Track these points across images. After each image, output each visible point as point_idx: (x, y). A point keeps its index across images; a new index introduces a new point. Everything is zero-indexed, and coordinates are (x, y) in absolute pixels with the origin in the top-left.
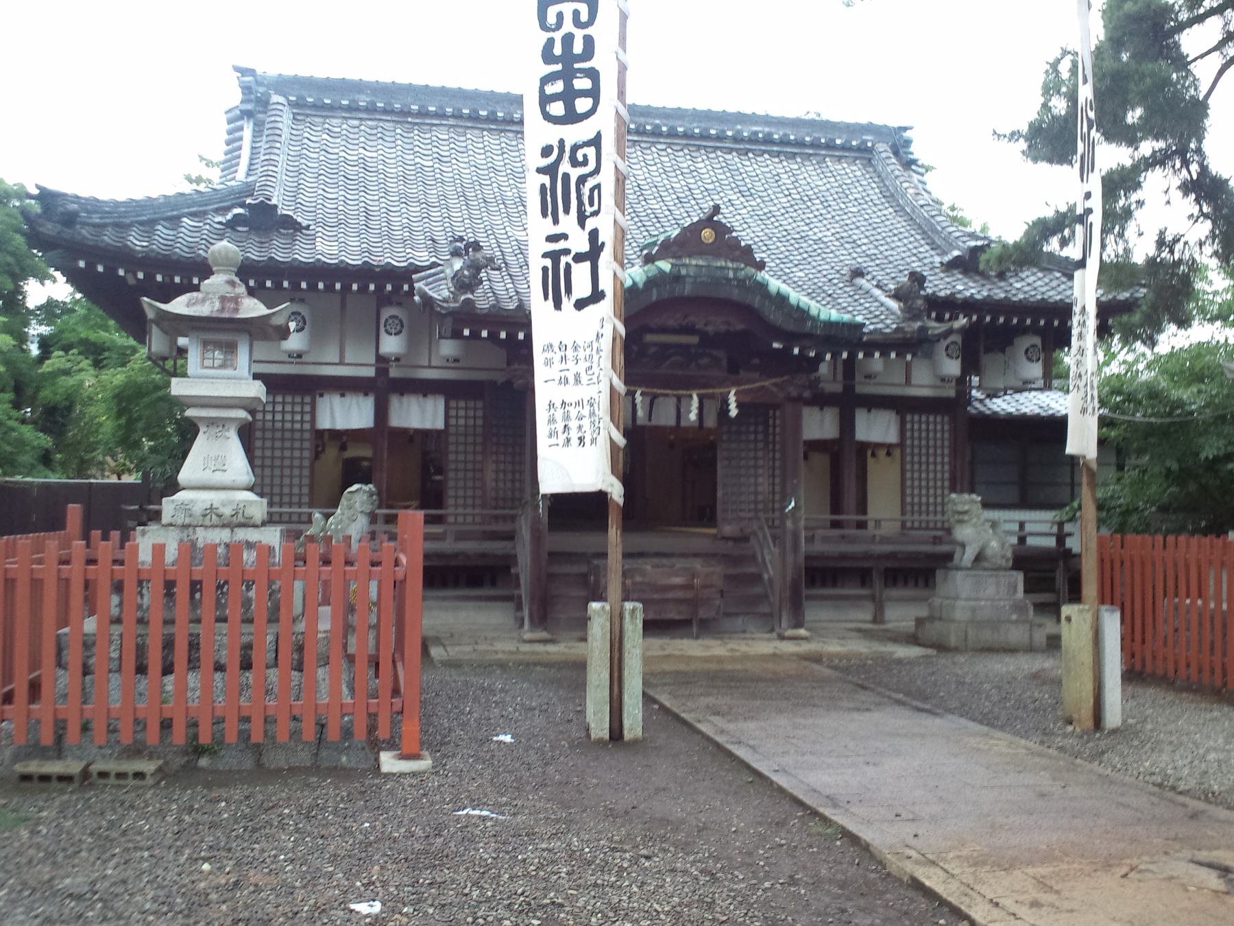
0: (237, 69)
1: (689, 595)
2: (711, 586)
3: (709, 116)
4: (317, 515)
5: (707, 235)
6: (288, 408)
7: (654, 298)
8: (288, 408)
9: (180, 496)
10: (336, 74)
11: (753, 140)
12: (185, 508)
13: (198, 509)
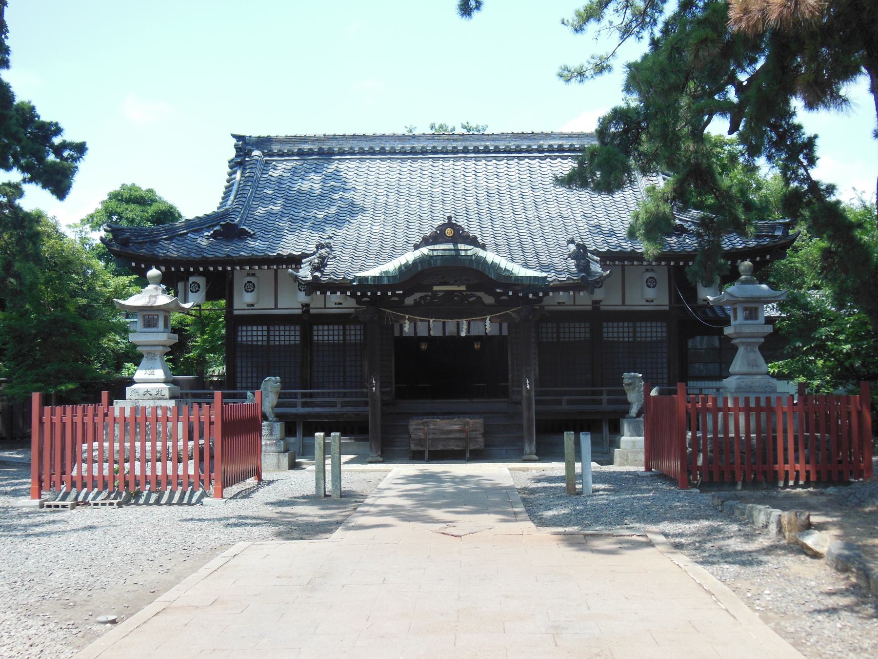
0: (234, 136)
1: (463, 436)
2: (476, 430)
3: (522, 136)
4: (249, 393)
5: (449, 232)
6: (282, 333)
7: (420, 269)
8: (282, 333)
9: (135, 386)
10: (291, 133)
11: (551, 150)
12: (136, 392)
13: (141, 392)
